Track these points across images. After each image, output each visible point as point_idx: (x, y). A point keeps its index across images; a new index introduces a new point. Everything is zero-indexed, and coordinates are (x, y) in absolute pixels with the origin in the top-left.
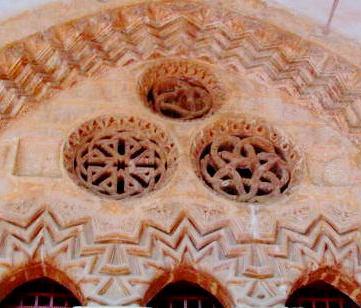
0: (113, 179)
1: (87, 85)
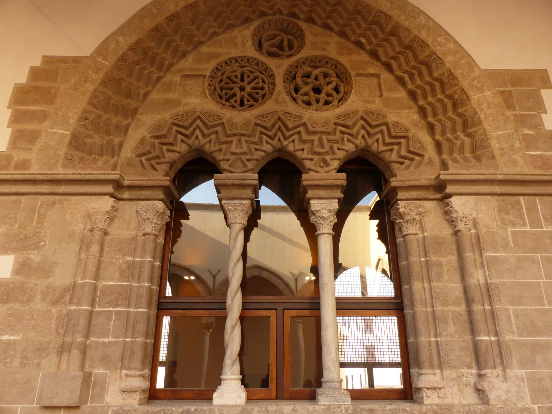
0: (238, 98)
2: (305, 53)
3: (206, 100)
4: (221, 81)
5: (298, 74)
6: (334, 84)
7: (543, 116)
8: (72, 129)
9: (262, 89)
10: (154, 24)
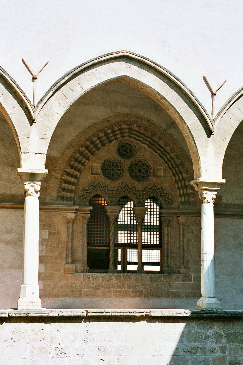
1: (105, 148)
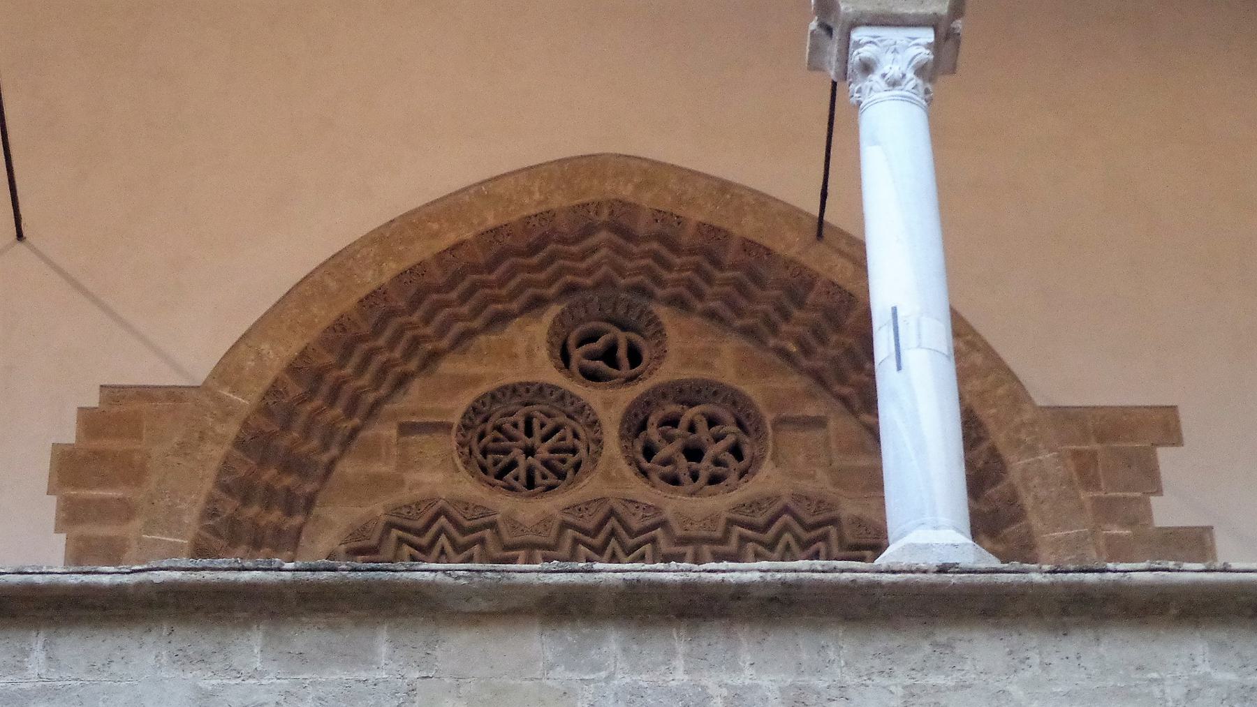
0: (521, 470)
2: (668, 372)
3: (457, 477)
4: (482, 436)
5: (652, 419)
6: (730, 439)
7: (1154, 500)
8: (191, 534)
9: (574, 451)
10: (335, 314)
